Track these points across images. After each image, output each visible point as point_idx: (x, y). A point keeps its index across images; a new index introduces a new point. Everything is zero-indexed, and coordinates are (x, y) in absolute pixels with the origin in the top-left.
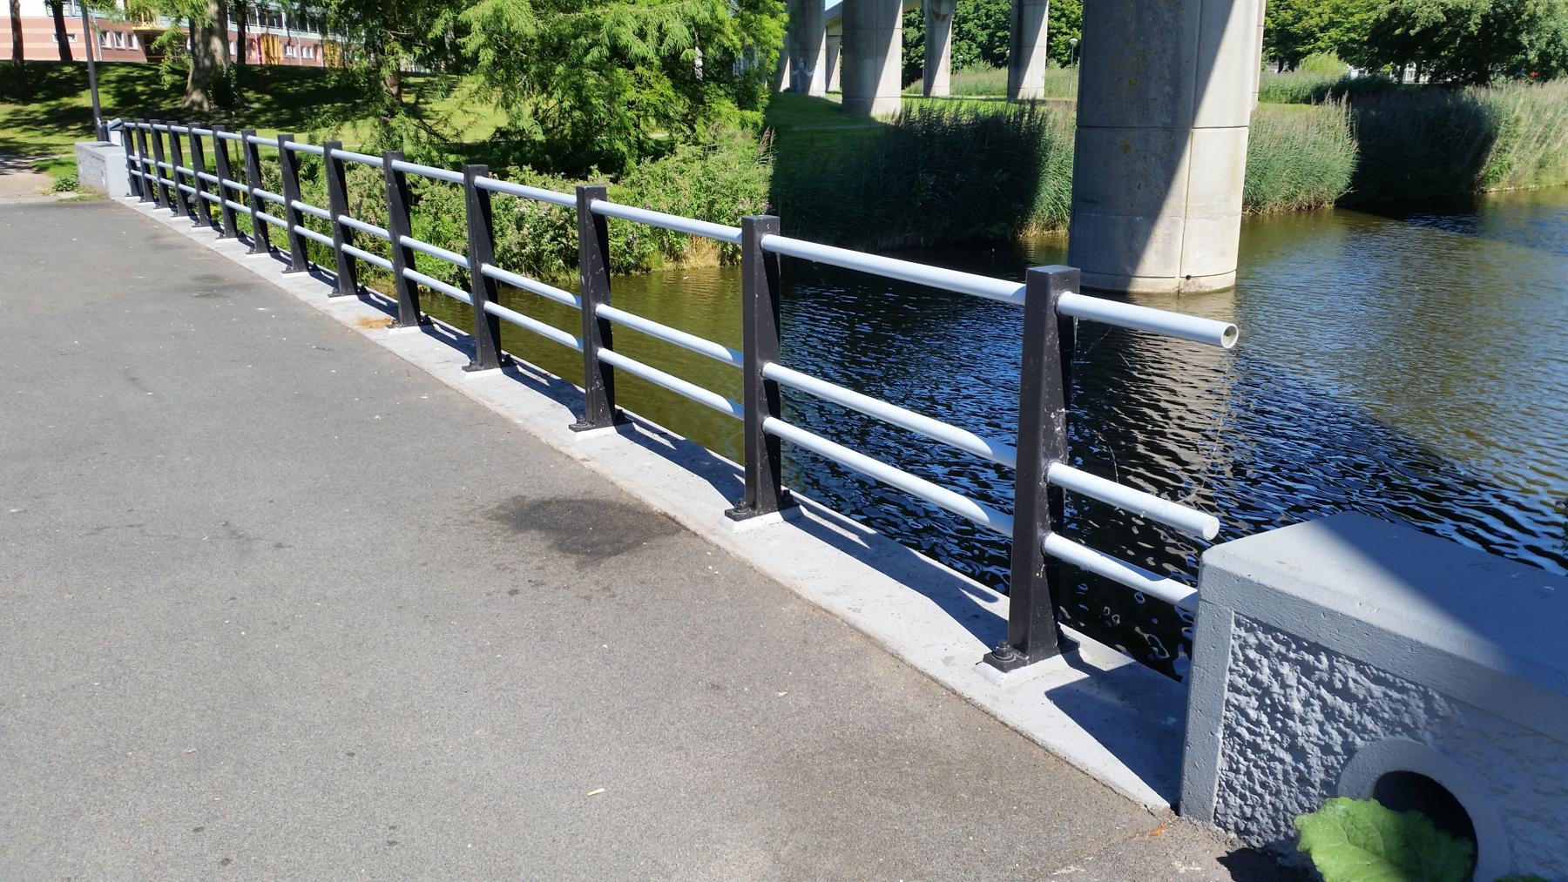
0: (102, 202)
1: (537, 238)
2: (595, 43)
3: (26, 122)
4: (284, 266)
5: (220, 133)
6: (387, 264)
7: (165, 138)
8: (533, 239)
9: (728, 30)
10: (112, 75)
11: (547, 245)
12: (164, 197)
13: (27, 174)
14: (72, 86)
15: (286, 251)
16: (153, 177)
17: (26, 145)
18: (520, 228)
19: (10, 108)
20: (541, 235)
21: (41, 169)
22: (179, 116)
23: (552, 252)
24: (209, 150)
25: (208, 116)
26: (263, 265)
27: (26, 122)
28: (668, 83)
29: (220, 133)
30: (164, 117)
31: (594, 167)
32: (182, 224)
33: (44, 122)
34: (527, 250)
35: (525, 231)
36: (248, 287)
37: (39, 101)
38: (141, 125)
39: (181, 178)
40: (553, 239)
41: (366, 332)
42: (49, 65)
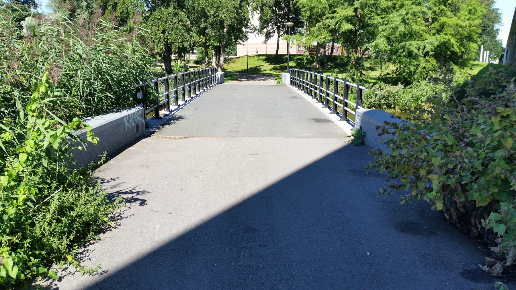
0: (285, 85)
1: (380, 100)
2: (404, 51)
3: (276, 69)
4: (340, 118)
5: (316, 74)
6: (342, 106)
7: (309, 75)
8: (379, 100)
9: (455, 47)
10: (296, 58)
11: (383, 101)
12: (299, 86)
13: (273, 80)
14: (286, 61)
15: (341, 114)
16: (324, 95)
17: (274, 74)
18: (376, 97)
19: (273, 66)
20: (381, 99)
21: (276, 80)
22: (310, 69)
23: (384, 104)
24: (313, 77)
25: (317, 69)
26: (334, 117)
27: (276, 69)
28: (435, 61)
29: (316, 74)
30: (306, 69)
31: (399, 83)
32: (305, 96)
33: (279, 69)
34: (376, 103)
35: (377, 98)
36: (300, 98)
37: (279, 64)
38: (304, 71)
39: (304, 82)
40: (385, 100)
41: (314, 104)
42: (284, 55)
